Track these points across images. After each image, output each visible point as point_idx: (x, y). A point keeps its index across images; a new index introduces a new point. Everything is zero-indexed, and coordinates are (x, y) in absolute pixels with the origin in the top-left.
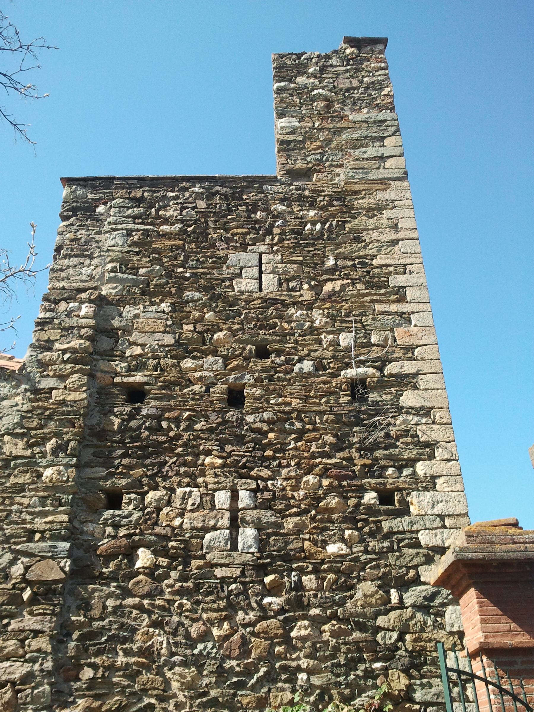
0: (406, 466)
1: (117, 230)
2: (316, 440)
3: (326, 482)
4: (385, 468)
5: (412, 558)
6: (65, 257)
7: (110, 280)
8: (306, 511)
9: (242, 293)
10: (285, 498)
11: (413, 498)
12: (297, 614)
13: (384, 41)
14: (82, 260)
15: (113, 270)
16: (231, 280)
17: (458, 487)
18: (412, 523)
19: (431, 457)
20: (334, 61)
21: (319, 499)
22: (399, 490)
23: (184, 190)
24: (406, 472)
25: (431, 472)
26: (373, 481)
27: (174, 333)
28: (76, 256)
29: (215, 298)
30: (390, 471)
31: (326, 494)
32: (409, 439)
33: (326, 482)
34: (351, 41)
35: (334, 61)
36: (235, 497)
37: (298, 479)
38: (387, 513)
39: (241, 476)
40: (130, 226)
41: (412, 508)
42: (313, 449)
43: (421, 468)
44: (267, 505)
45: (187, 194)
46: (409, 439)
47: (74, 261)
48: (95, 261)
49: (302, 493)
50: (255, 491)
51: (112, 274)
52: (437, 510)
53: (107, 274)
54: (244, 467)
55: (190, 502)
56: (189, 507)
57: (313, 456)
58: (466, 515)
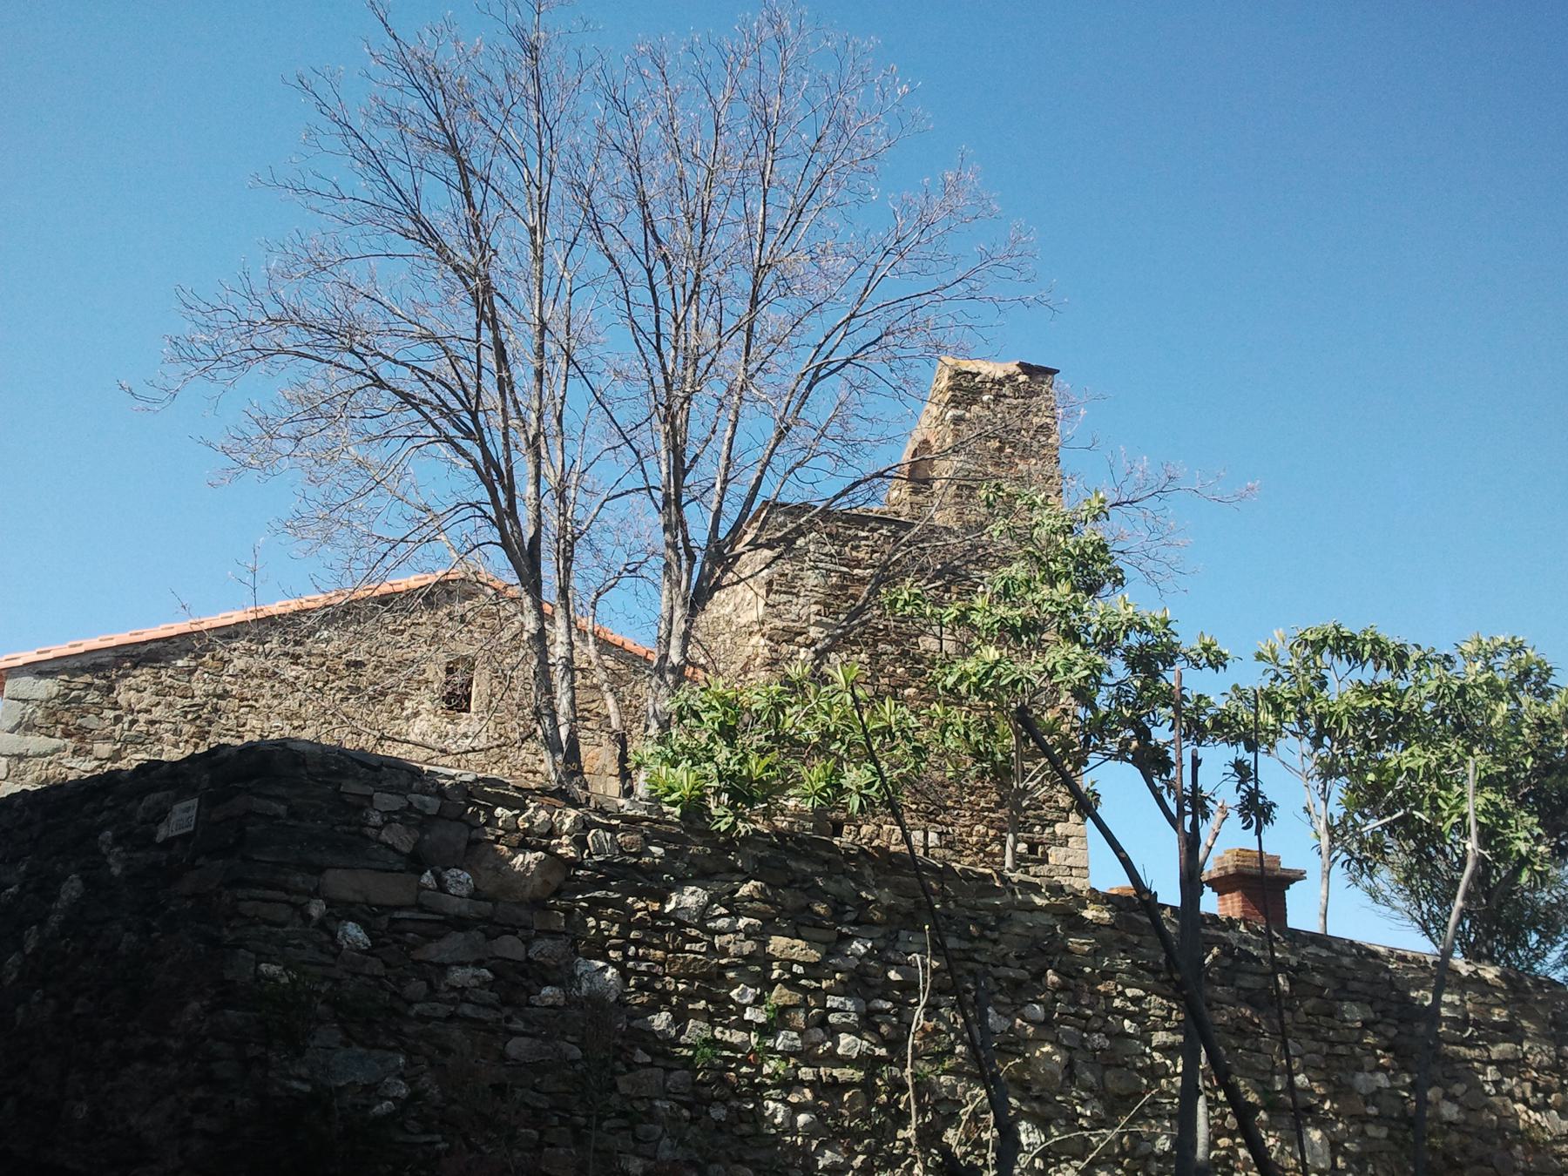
0: (1048, 825)
1: (817, 568)
2: (984, 796)
3: (991, 833)
4: (1034, 825)
5: (471, 205)
6: (777, 592)
7: (817, 624)
8: (977, 854)
9: (927, 651)
10: (961, 841)
11: (1052, 851)
12: (1211, 956)
13: (1054, 372)
14: (790, 598)
15: (818, 613)
16: (917, 636)
17: (1084, 846)
18: (1050, 870)
19: (1067, 820)
20: (1006, 390)
21: (987, 845)
22: (1042, 844)
23: (872, 530)
24: (1048, 830)
25: (1066, 832)
26: (1026, 835)
27: (873, 685)
28: (785, 593)
29: (905, 653)
30: (1037, 828)
31: (992, 841)
32: (1052, 804)
33: (991, 833)
34: (1026, 368)
35: (1006, 390)
36: (926, 837)
37: (971, 826)
38: (1034, 861)
39: (930, 821)
40: (830, 566)
41: (1050, 859)
42: (982, 804)
43: (1059, 828)
44: (949, 845)
45: (876, 535)
46: (1052, 804)
47: (784, 598)
48: (801, 600)
49: (975, 839)
50: (940, 834)
51: (818, 618)
52: (1068, 862)
53: (812, 616)
54: (931, 813)
55: (894, 838)
56: (893, 842)
57: (983, 809)
58: (1086, 868)
